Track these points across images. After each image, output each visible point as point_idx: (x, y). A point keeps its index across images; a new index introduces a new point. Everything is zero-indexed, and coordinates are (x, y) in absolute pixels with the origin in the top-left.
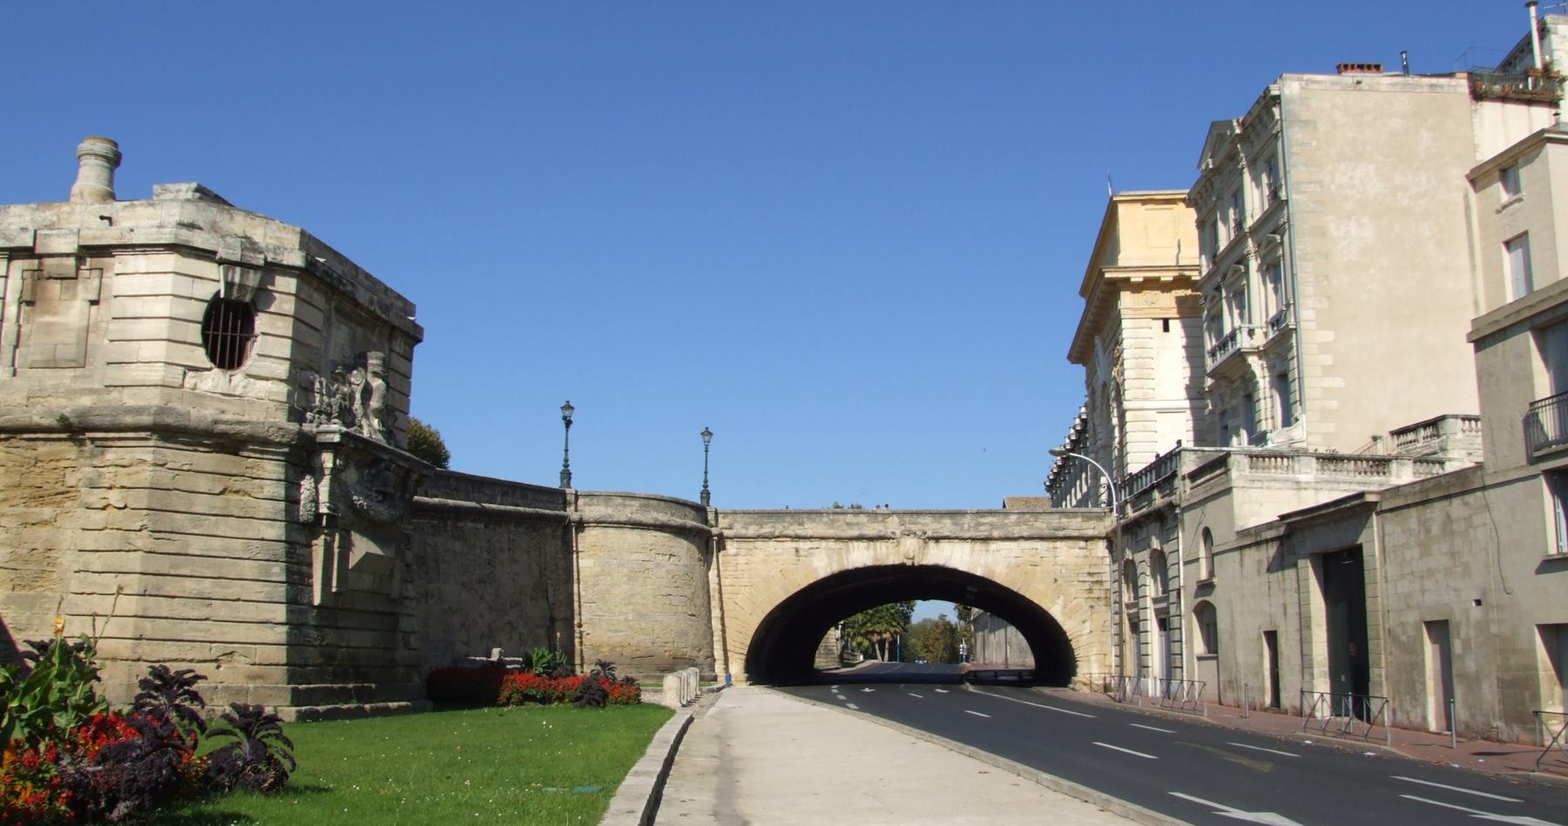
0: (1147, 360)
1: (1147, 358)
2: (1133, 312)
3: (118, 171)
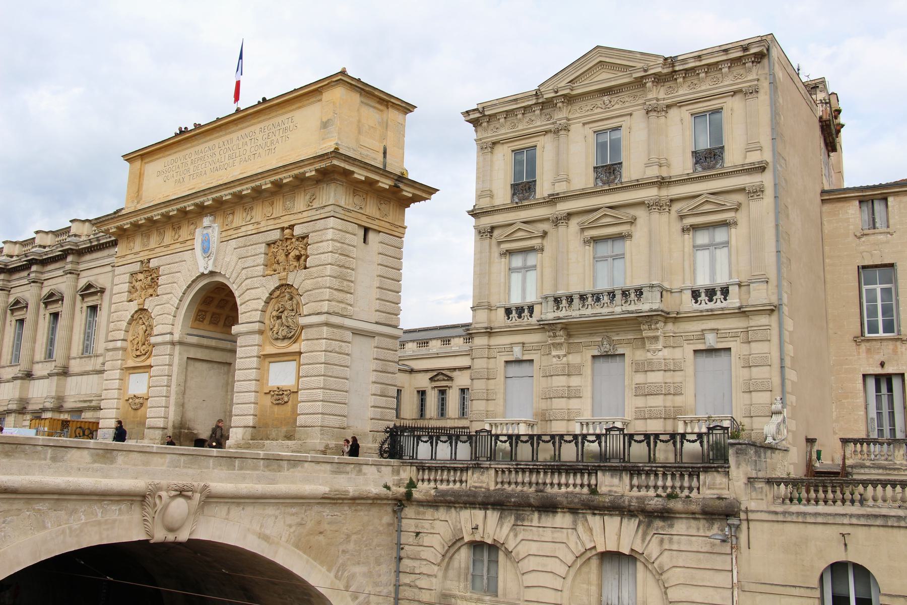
0: (349, 271)
1: (349, 268)
2: (343, 212)
3: (543, 253)
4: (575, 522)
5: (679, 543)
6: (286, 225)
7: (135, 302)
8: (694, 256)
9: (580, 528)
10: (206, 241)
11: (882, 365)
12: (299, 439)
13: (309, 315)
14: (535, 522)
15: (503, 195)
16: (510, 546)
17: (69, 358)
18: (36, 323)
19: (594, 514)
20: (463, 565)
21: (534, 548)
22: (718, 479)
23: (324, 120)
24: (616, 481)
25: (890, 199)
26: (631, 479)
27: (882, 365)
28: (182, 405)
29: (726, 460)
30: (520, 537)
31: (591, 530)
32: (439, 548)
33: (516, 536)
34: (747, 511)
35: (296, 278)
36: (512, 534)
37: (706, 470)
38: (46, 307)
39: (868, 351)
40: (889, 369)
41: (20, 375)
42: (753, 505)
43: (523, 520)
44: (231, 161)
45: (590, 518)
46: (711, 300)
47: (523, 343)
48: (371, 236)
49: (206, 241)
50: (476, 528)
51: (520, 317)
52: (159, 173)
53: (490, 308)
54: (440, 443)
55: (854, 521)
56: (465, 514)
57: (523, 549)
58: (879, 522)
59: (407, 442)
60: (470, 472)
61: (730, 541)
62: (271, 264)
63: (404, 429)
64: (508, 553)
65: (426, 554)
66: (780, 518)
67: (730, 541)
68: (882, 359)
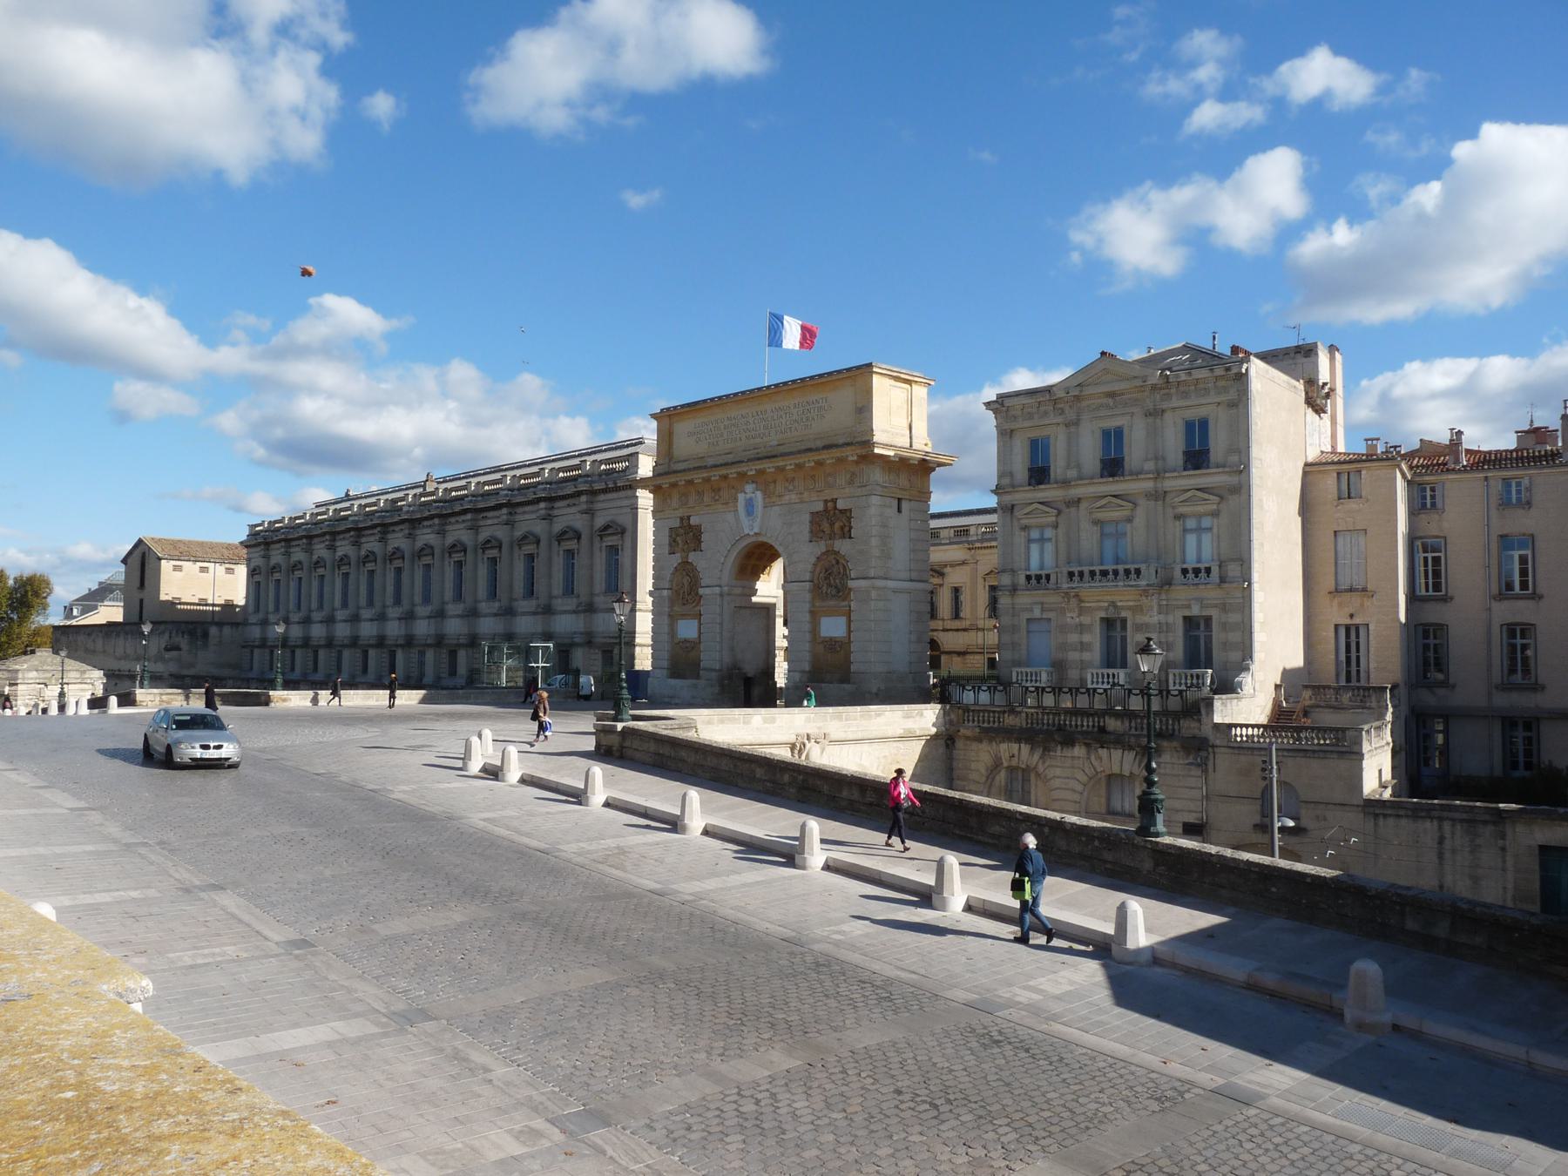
4: (1088, 753)
5: (1165, 768)
6: (829, 498)
7: (678, 555)
8: (1184, 537)
9: (1093, 757)
10: (750, 504)
11: (1352, 616)
12: (854, 683)
13: (857, 579)
14: (1059, 753)
15: (1021, 472)
16: (1041, 768)
17: (592, 594)
18: (550, 559)
19: (1103, 747)
20: (1003, 783)
21: (1058, 772)
22: (1194, 724)
23: (859, 405)
24: (1119, 723)
25: (1363, 472)
26: (1130, 722)
27: (1352, 616)
28: (732, 649)
29: (1199, 711)
30: (1047, 764)
31: (1101, 759)
32: (983, 771)
33: (1044, 762)
34: (1213, 746)
35: (843, 546)
36: (1041, 761)
37: (1185, 717)
38: (559, 544)
39: (1340, 605)
40: (1357, 621)
41: (540, 610)
42: (1218, 742)
43: (1049, 751)
44: (767, 431)
45: (1100, 750)
46: (1197, 577)
47: (1042, 603)
48: (905, 505)
49: (750, 504)
50: (1013, 756)
51: (1038, 583)
52: (690, 434)
53: (1013, 571)
54: (981, 692)
55: (1286, 754)
56: (1004, 746)
57: (1051, 773)
58: (1301, 754)
59: (954, 689)
60: (1006, 715)
61: (1203, 766)
62: (816, 533)
63: (1113, 774)
64: (1038, 775)
65: (974, 776)
66: (1236, 752)
67: (1203, 766)
68: (1352, 611)
